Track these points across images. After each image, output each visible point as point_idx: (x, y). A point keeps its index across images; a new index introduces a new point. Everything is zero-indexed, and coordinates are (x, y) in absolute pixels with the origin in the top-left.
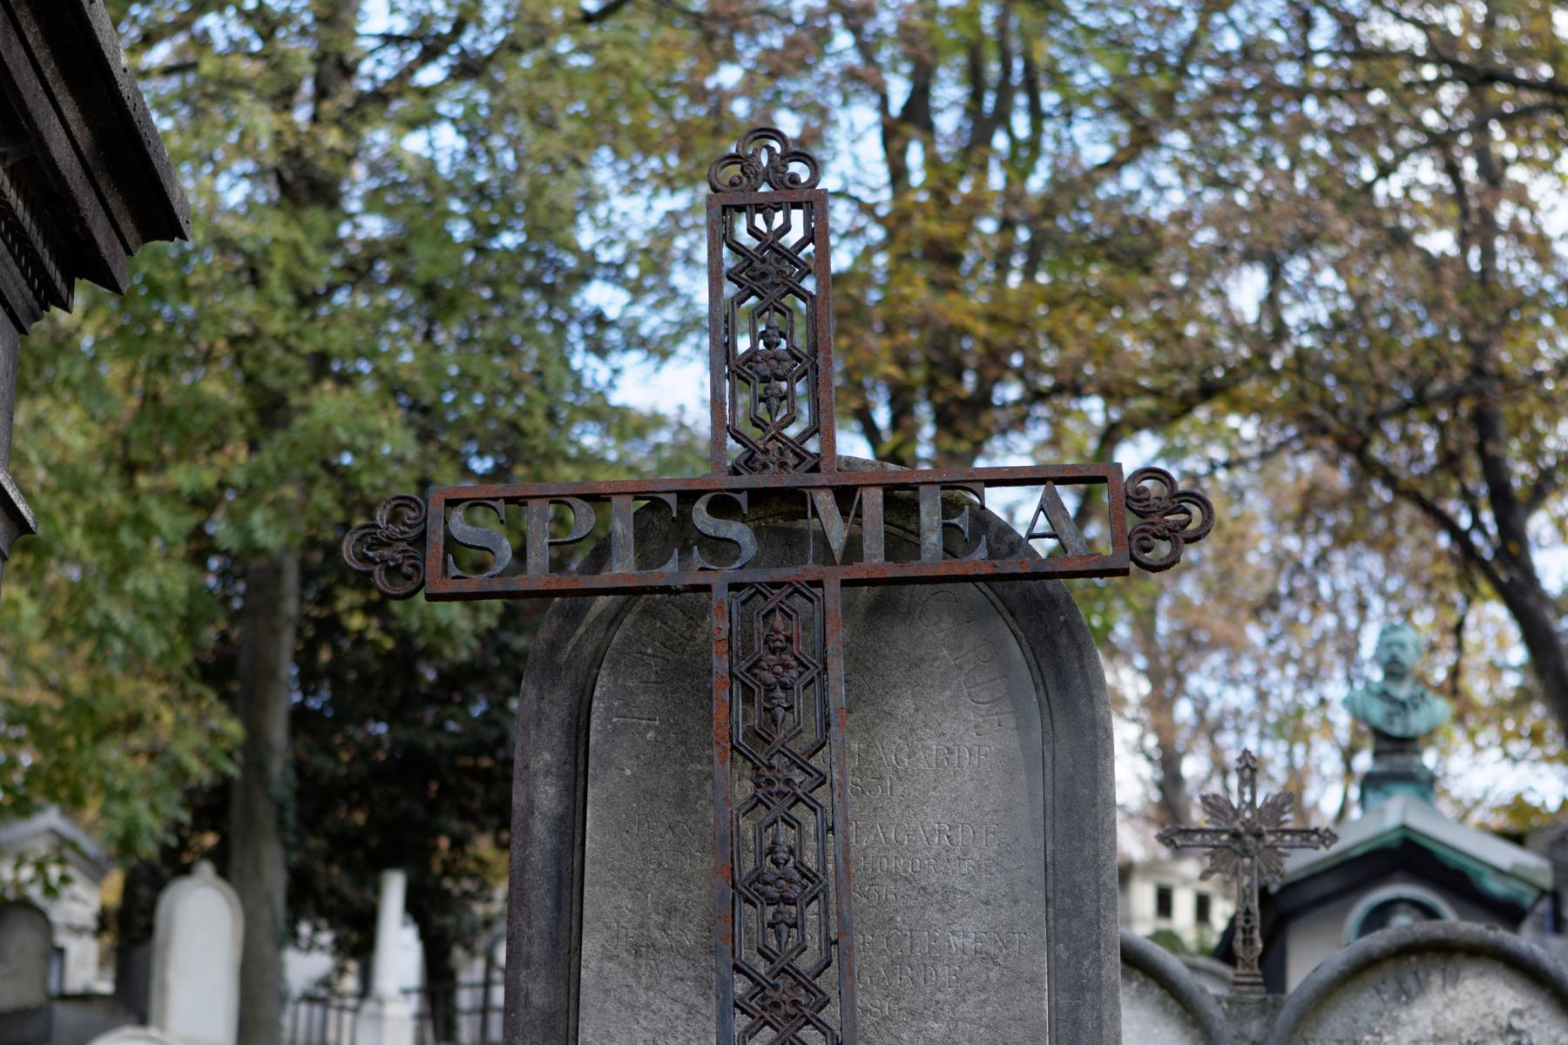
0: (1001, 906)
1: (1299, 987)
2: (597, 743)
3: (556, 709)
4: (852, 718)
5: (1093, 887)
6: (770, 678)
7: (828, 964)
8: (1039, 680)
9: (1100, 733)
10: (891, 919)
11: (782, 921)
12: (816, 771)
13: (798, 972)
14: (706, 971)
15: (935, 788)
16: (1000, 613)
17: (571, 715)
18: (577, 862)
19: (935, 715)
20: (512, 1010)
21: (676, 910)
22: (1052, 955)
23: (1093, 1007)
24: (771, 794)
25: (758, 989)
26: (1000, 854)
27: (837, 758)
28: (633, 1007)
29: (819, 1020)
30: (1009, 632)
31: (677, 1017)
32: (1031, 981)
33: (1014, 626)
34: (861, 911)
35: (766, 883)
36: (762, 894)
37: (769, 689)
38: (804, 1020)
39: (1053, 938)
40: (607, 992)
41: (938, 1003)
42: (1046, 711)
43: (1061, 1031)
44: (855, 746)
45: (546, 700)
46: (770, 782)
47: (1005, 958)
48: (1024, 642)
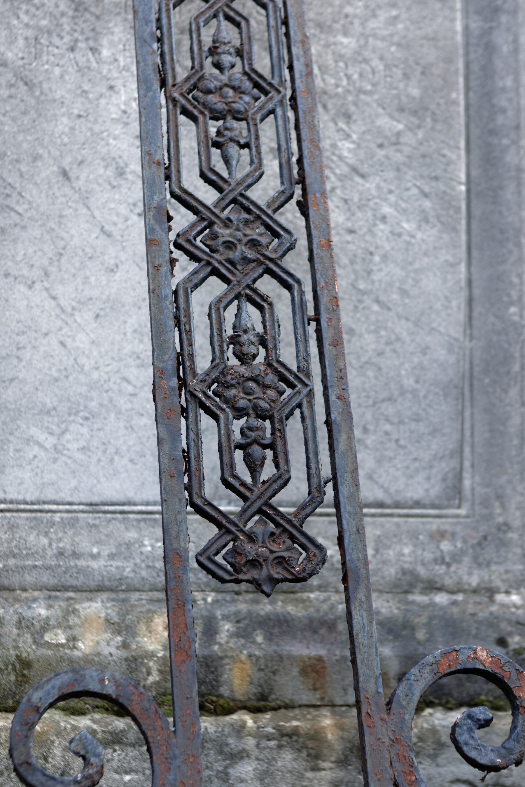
31: (63, 14)
35: (209, 92)
41: (347, 16)
43: (472, 56)
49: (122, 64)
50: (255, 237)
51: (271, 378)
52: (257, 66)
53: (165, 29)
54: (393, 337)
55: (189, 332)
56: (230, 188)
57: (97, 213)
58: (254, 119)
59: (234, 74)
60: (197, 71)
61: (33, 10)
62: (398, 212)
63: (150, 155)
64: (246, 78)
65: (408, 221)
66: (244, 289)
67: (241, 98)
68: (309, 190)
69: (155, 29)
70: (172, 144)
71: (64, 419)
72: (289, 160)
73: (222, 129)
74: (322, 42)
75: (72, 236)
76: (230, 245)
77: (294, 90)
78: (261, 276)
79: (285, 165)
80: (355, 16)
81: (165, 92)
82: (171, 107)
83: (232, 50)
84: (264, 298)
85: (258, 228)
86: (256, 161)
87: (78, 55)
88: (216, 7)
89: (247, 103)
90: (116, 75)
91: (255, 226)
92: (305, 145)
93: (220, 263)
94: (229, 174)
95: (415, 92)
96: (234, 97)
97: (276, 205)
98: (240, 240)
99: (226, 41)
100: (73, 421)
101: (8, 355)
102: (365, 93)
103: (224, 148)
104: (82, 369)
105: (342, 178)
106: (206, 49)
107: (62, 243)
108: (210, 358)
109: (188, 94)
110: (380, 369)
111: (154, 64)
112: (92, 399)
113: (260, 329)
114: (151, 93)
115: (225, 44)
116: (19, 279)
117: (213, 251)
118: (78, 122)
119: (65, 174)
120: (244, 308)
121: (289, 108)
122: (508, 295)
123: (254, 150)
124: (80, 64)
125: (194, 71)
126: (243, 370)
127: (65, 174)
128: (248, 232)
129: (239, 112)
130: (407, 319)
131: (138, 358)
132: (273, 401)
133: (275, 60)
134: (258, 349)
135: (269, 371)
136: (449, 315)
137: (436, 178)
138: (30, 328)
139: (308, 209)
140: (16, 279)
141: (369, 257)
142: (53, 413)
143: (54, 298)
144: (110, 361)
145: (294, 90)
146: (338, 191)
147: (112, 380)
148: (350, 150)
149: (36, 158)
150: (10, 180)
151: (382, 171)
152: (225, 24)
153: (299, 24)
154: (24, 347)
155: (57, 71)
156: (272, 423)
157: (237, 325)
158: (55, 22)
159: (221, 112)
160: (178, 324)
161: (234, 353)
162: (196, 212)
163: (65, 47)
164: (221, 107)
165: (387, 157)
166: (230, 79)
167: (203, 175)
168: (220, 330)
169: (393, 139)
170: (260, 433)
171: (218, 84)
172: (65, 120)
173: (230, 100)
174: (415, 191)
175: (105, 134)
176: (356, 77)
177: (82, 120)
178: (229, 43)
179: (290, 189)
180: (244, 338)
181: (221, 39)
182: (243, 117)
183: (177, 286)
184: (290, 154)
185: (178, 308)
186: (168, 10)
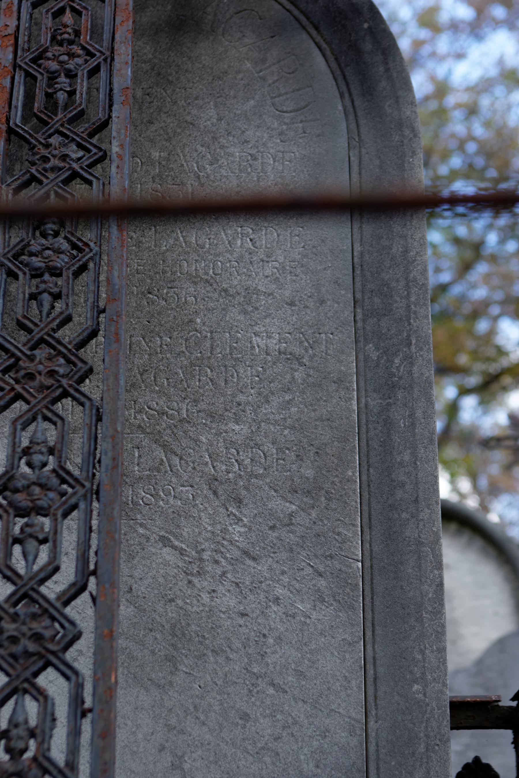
0: (306, 307)
1: (502, 706)
4: (153, 128)
5: (402, 283)
6: (54, 66)
8: (344, 88)
9: (407, 132)
10: (191, 321)
11: (44, 291)
13: (59, 342)
16: (304, 28)
19: (238, 124)
22: (361, 357)
23: (405, 405)
25: (13, 360)
26: (306, 256)
27: (118, 133)
30: (313, 45)
32: (339, 381)
33: (319, 39)
34: (159, 314)
35: (16, 491)
36: (26, 265)
37: (53, 77)
38: (60, 390)
39: (362, 339)
41: (239, 404)
42: (352, 117)
43: (372, 433)
44: (156, 154)
46: (45, 159)
47: (311, 358)
48: (328, 53)
50: (40, 630)
54: (290, 721)
56: (22, 583)
62: (291, 592)
65: (302, 601)
66: (22, 682)
67: (46, 495)
74: (213, 431)
80: (248, 403)
89: (51, 500)
95: (309, 473)
97: (66, 598)
98: (24, 635)
102: (256, 477)
105: (233, 562)
110: (277, 754)
115: (38, 444)
122: (411, 672)
129: (42, 508)
130: (305, 702)
136: (348, 695)
137: (331, 557)
141: (262, 639)
146: (229, 576)
148: (240, 534)
151: (275, 553)
159: (25, 510)
165: (279, 539)
166: (38, 478)
169: (286, 521)
173: (35, 497)
174: (309, 570)
176: (247, 461)
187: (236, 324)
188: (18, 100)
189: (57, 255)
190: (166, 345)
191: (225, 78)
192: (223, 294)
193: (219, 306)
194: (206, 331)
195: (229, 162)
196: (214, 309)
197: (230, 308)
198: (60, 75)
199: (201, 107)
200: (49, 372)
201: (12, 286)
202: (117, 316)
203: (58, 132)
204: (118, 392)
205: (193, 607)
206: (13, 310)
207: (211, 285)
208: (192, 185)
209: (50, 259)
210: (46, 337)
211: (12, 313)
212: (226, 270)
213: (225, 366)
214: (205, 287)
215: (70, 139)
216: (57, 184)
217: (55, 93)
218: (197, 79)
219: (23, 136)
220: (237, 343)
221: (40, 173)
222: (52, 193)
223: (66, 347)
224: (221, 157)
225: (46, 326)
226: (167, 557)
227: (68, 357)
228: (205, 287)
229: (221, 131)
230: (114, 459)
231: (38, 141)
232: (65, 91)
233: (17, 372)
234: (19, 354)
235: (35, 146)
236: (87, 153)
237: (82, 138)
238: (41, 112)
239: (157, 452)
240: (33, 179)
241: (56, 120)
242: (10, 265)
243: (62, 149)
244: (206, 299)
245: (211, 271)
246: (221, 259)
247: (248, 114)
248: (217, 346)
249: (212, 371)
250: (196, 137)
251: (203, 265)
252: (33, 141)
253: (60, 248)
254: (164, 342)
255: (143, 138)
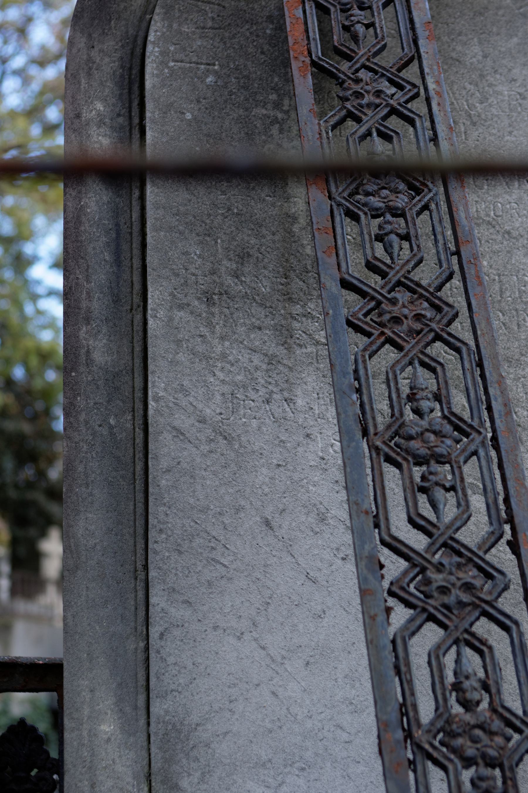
2: (154, 86)
3: (107, 60)
7: (450, 277)
11: (391, 232)
12: (408, 82)
14: (285, 319)
15: (510, 133)
17: (122, 67)
18: (136, 215)
20: (72, 369)
21: (249, 255)
24: (362, 107)
25: (373, 304)
27: (431, 69)
28: (208, 358)
29: (450, 334)
31: (257, 368)
35: (410, 438)
36: (365, 205)
38: (432, 335)
40: (178, 343)
45: (96, 49)
49: (317, 412)
50: (469, 580)
51: (497, 724)
52: (457, 410)
53: (363, 380)
55: (410, 682)
56: (440, 532)
57: (301, 560)
58: (457, 462)
59: (433, 419)
60: (397, 419)
61: (228, 366)
63: (357, 504)
64: (446, 421)
66: (462, 633)
67: (442, 442)
68: (518, 528)
69: (353, 380)
70: (378, 493)
71: (280, 771)
72: (496, 500)
73: (426, 474)
75: (278, 585)
76: (444, 590)
77: (494, 431)
78: (478, 619)
79: (492, 506)
81: (367, 441)
82: (374, 455)
83: (430, 396)
84: (483, 642)
85: (470, 570)
86: (463, 503)
87: (274, 406)
88: (410, 355)
90: (312, 423)
91: (467, 569)
92: (511, 484)
93: (436, 608)
94: (438, 518)
96: (436, 441)
98: (453, 585)
99: (424, 387)
100: (289, 773)
101: (220, 708)
103: (430, 493)
104: (295, 718)
106: (404, 396)
107: (269, 592)
108: (433, 707)
109: (390, 441)
111: (355, 414)
112: (307, 749)
113: (481, 674)
114: (354, 444)
115: (422, 390)
116: (228, 631)
117: (428, 596)
118: (277, 471)
119: (267, 523)
120: (463, 653)
121: (491, 448)
123: (460, 492)
124: (276, 415)
125: (394, 418)
126: (468, 717)
127: (267, 523)
128: (461, 575)
129: (442, 456)
131: (352, 703)
132: (502, 748)
133: (473, 402)
134: (481, 695)
135: (494, 717)
138: (241, 679)
139: (519, 548)
140: (225, 630)
142: (269, 765)
143: (263, 648)
144: (323, 709)
145: (494, 431)
147: (326, 728)
149: (238, 510)
150: (214, 533)
152: (420, 370)
153: (493, 364)
154: (236, 700)
155: (254, 423)
156: (503, 771)
157: (458, 670)
158: (250, 377)
159: (424, 458)
160: (398, 672)
161: (458, 701)
162: (407, 558)
163: (260, 400)
164: (424, 452)
166: (430, 424)
167: (411, 521)
168: (442, 678)
170: (491, 783)
171: (419, 430)
172: (264, 471)
173: (432, 444)
175: (305, 481)
177: (281, 469)
178: (426, 388)
179: (499, 529)
180: (467, 684)
181: (418, 386)
182: (446, 460)
183: (395, 635)
184: (496, 495)
185: (397, 657)
186: (364, 362)
187: (522, 267)
188: (314, 32)
189: (395, 195)
190: (456, 288)
191: (486, 14)
192: (506, 236)
193: (503, 248)
194: (494, 274)
195: (499, 100)
196: (499, 252)
197: (515, 251)
198: (352, 7)
199: (465, 44)
200: (415, 315)
201: (295, 226)
202: (474, 259)
203: (364, 66)
204: (493, 336)
205: (506, 554)
206: (298, 252)
207: (494, 227)
208: (464, 124)
209: (388, 199)
210: (403, 279)
211: (298, 254)
212: (507, 212)
213: (516, 310)
214: (488, 229)
215: (380, 74)
216: (377, 121)
217: (353, 25)
218: (458, 14)
219: (330, 70)
220: (525, 286)
221: (357, 109)
222: (374, 130)
223: (427, 290)
224: (490, 95)
225: (401, 269)
226: (477, 504)
227: (431, 300)
228: (488, 229)
229: (487, 68)
230: (505, 405)
231: (346, 75)
232: (363, 24)
233: (380, 315)
234: (380, 297)
235: (344, 82)
236: (399, 91)
237: (392, 74)
238: (342, 45)
239: (458, 398)
240: (350, 115)
241: (360, 54)
242: (347, 204)
243: (374, 85)
244: (491, 241)
245: (492, 213)
246: (500, 200)
247: (513, 51)
248: (506, 289)
249: (504, 315)
250: (463, 74)
251: (483, 206)
252: (341, 76)
253: (397, 188)
254: (453, 285)
255: (411, 74)
